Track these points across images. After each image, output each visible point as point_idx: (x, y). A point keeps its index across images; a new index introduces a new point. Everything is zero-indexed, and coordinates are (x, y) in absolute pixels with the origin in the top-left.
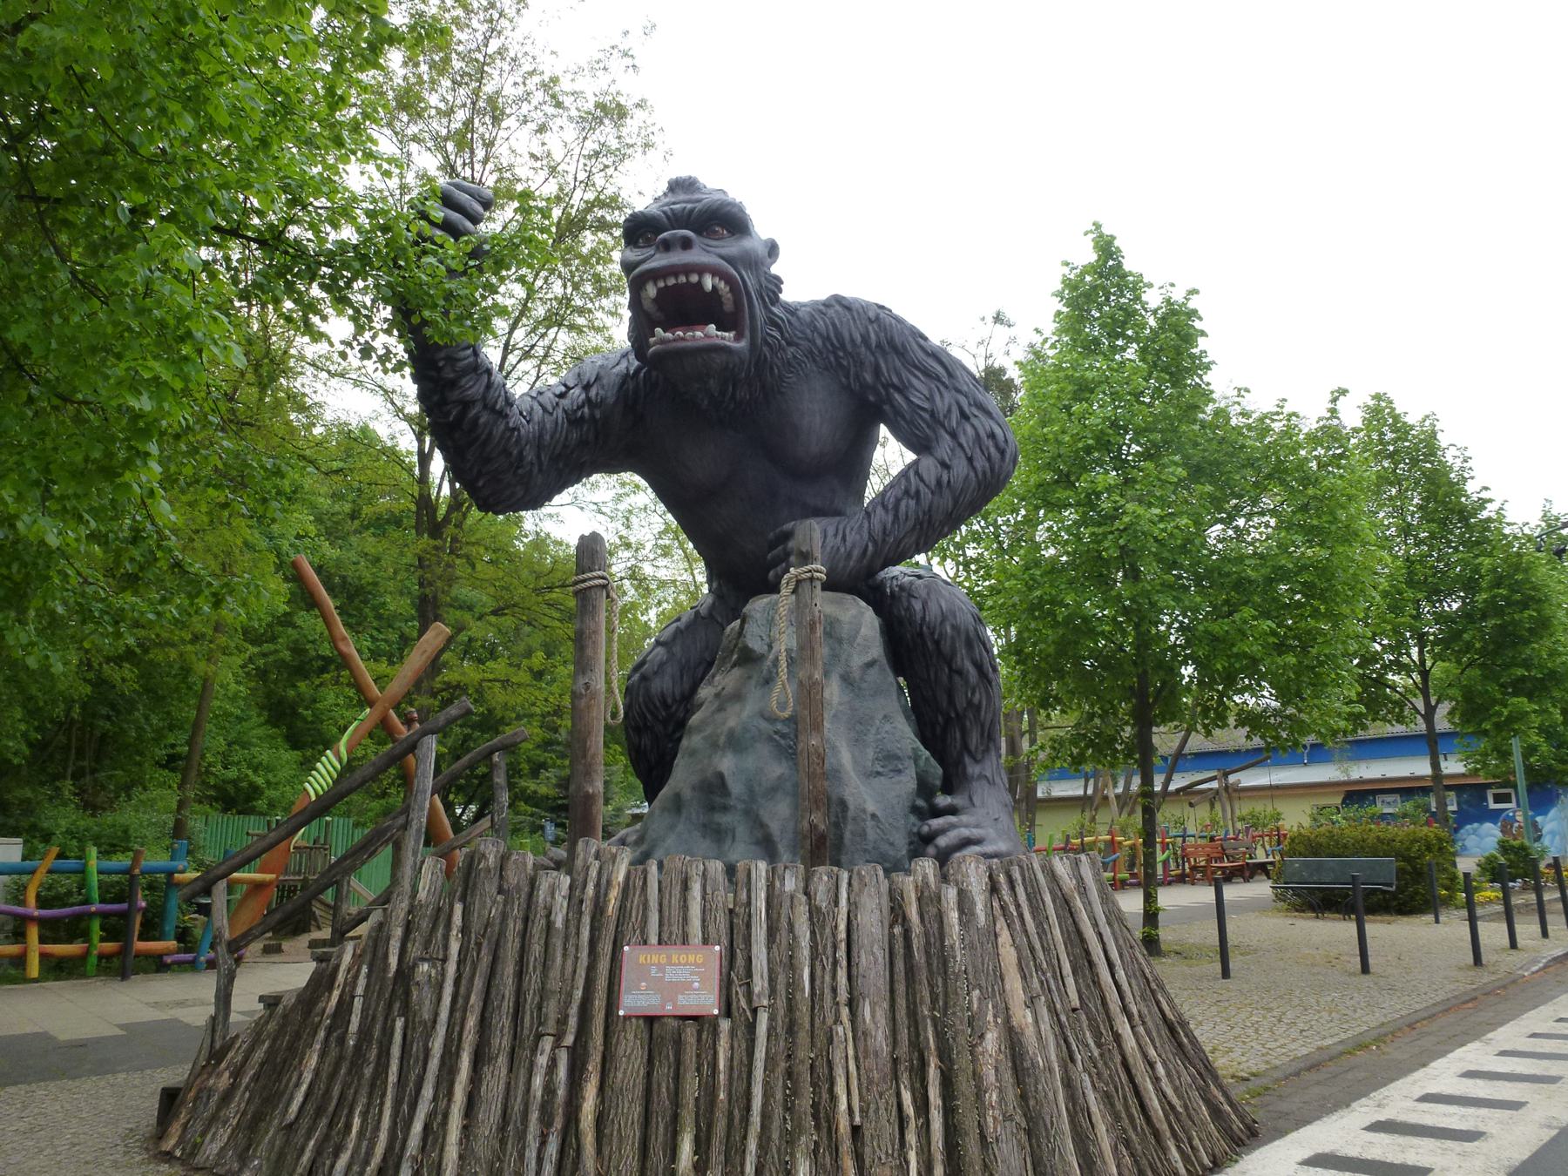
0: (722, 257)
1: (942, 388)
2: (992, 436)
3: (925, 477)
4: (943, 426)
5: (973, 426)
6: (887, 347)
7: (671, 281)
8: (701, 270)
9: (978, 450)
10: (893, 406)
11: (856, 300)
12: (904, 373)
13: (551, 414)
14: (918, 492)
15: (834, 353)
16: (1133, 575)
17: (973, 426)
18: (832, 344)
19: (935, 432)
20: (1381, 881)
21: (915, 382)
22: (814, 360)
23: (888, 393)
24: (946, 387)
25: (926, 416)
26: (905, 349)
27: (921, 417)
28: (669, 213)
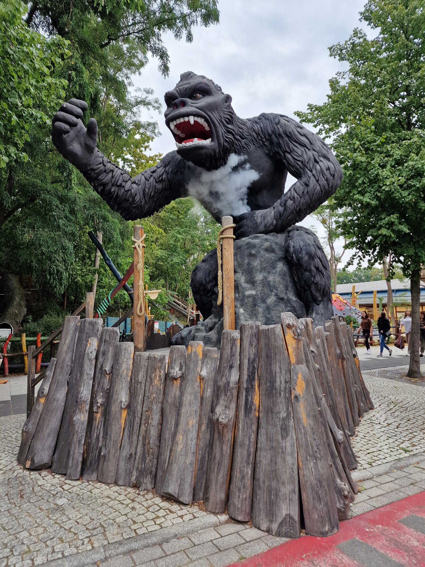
0: (197, 108)
1: (307, 150)
2: (328, 169)
3: (297, 191)
4: (307, 167)
5: (320, 166)
6: (283, 135)
7: (182, 120)
8: (188, 115)
9: (322, 176)
10: (287, 160)
11: (272, 114)
12: (291, 145)
13: (148, 180)
14: (294, 197)
15: (261, 140)
16: (93, 221)
17: (320, 166)
18: (261, 137)
19: (303, 169)
20: (225, 294)
21: (295, 148)
22: (254, 144)
23: (285, 155)
24: (309, 150)
25: (300, 163)
26: (292, 135)
27: (297, 164)
28: (178, 91)
